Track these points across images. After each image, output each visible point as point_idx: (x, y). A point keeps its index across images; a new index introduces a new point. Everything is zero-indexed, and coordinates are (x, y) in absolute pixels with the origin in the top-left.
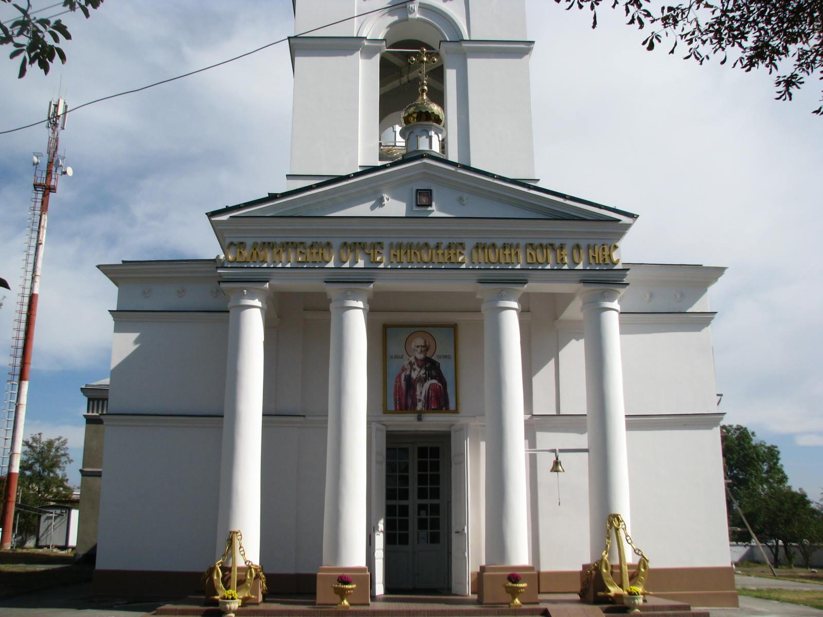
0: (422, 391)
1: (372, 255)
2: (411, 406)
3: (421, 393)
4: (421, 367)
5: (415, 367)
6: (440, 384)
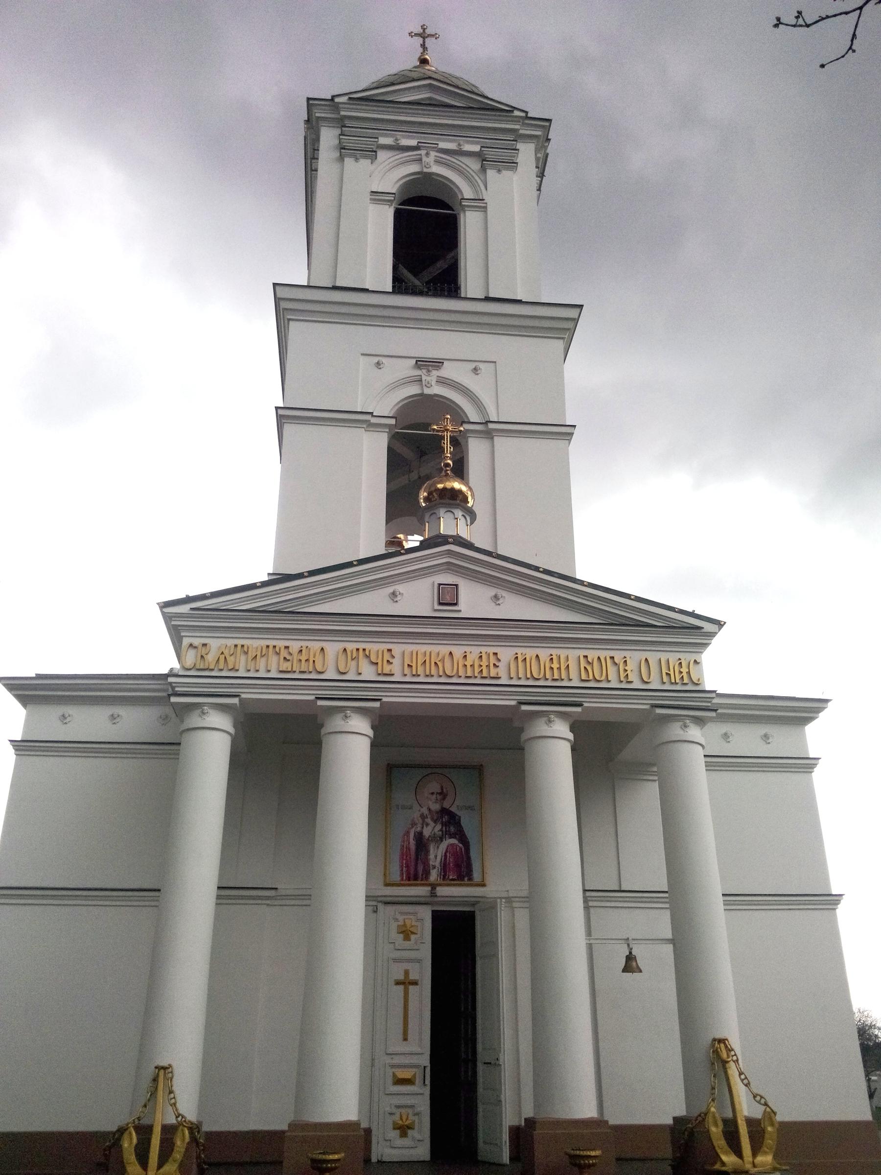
0: (436, 854)
1: (380, 665)
2: (422, 875)
3: (436, 857)
4: (435, 822)
5: (429, 820)
6: (461, 845)
